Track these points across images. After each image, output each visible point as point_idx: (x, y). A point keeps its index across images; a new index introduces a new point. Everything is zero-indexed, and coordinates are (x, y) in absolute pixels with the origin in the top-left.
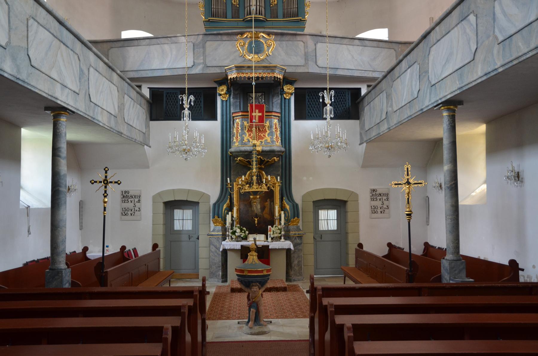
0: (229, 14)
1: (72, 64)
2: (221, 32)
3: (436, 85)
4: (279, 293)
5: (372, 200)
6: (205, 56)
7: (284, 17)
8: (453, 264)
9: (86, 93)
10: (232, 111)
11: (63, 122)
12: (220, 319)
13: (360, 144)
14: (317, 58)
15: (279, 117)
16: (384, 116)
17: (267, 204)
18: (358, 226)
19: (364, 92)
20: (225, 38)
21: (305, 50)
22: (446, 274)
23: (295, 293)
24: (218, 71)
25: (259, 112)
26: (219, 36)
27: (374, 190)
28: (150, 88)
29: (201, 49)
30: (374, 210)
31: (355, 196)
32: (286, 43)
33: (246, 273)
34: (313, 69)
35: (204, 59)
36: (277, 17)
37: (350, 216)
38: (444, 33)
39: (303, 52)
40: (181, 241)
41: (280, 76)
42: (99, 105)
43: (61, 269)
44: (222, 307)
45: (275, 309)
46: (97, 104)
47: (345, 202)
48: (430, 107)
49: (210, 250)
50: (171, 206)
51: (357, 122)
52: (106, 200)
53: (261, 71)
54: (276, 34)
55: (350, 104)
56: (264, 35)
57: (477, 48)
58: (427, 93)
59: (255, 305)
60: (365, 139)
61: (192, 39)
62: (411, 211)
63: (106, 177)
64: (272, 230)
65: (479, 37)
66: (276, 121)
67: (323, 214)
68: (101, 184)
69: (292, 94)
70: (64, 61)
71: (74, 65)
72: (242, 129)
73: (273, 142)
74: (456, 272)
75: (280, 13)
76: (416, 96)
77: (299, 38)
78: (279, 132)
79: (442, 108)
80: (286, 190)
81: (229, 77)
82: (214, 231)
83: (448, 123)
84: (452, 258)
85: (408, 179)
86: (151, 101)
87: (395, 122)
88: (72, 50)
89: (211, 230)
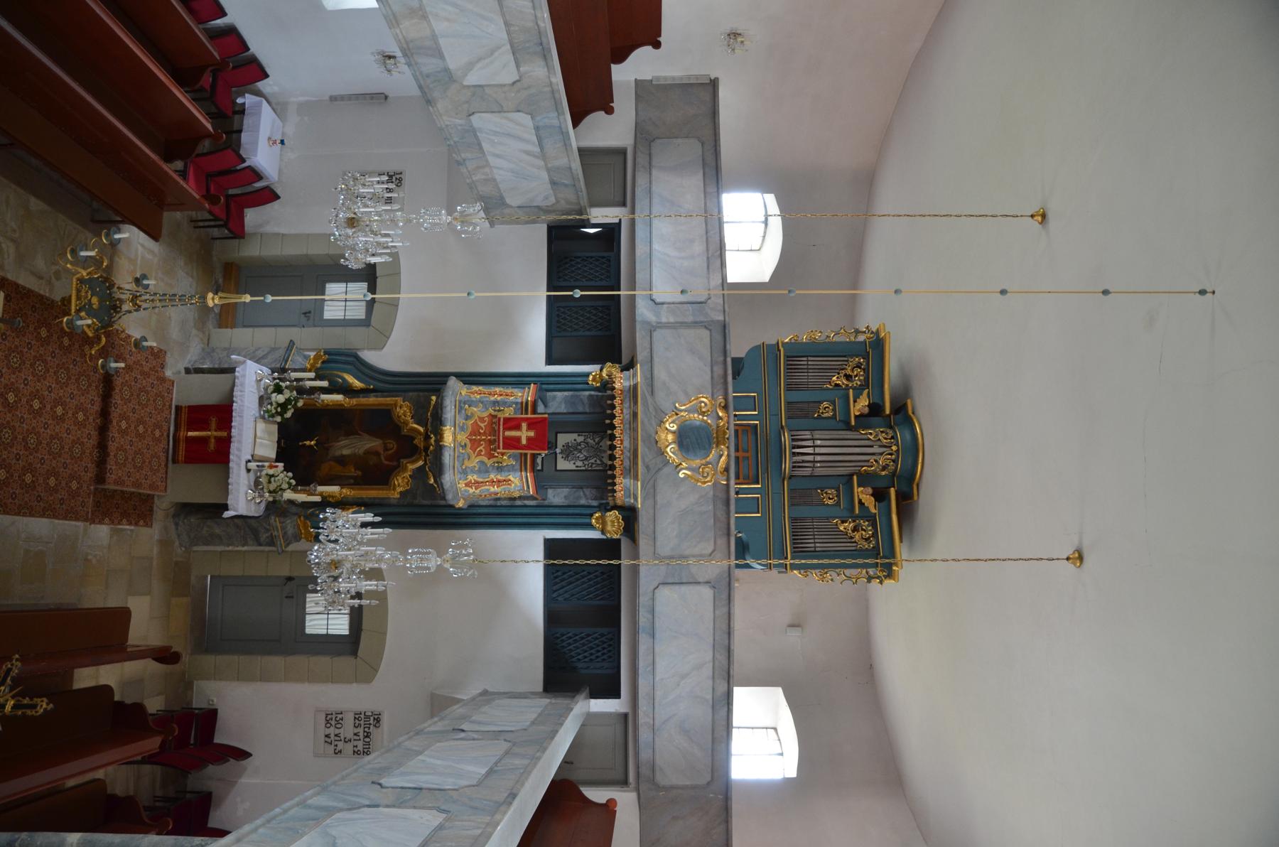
0: (796, 396)
5: (357, 716)
6: (675, 328)
14: (677, 587)
17: (352, 471)
18: (300, 680)
21: (694, 556)
25: (529, 439)
27: (378, 720)
28: (619, 224)
29: (691, 319)
30: (333, 719)
31: (367, 674)
36: (792, 505)
39: (687, 552)
47: (354, 653)
51: (540, 688)
53: (626, 443)
56: (723, 458)
64: (281, 475)
73: (464, 472)
75: (803, 511)
77: (722, 542)
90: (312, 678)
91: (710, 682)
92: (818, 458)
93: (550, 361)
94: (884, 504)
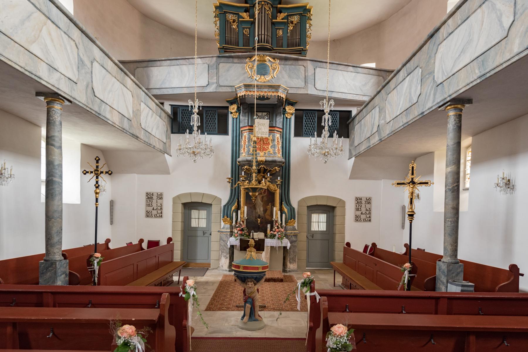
1: (66, 49)
2: (233, 54)
3: (444, 83)
4: (276, 283)
6: (219, 77)
7: (288, 47)
8: (451, 266)
9: (87, 86)
10: (241, 126)
11: (57, 109)
12: (220, 309)
13: (349, 159)
15: (281, 132)
16: (375, 129)
17: (269, 207)
18: (344, 227)
19: (354, 113)
20: (236, 60)
22: (443, 277)
23: (290, 283)
24: (229, 90)
26: (231, 59)
28: (171, 105)
29: (215, 70)
31: (342, 203)
32: (289, 66)
33: (241, 270)
34: (311, 91)
35: (218, 79)
36: (282, 47)
37: (338, 220)
38: (459, 22)
39: (304, 76)
40: (198, 236)
41: (283, 96)
42: (108, 103)
43: (56, 261)
44: (225, 296)
45: (272, 300)
46: (105, 101)
47: (333, 208)
48: (434, 108)
49: (220, 244)
50: (189, 206)
52: (98, 191)
53: (266, 90)
54: (281, 59)
55: (344, 124)
57: (514, 21)
58: (430, 94)
59: (250, 300)
60: (354, 154)
61: (207, 60)
62: (413, 212)
63: (97, 167)
65: (518, 7)
66: (278, 135)
67: (315, 217)
68: (93, 174)
69: (292, 114)
70: (52, 40)
71: (69, 51)
72: (249, 142)
73: (275, 153)
74: (454, 275)
76: (415, 102)
77: (300, 63)
78: (280, 146)
79: (449, 107)
80: (285, 198)
81: (238, 96)
82: (223, 228)
83: (454, 123)
84: (450, 261)
85: (412, 179)
86: (172, 116)
87: (388, 132)
88: (65, 33)
89: (222, 227)
90: (343, 224)
91: (349, 73)
92: (266, 33)
93: (228, 134)
94: (283, 11)
